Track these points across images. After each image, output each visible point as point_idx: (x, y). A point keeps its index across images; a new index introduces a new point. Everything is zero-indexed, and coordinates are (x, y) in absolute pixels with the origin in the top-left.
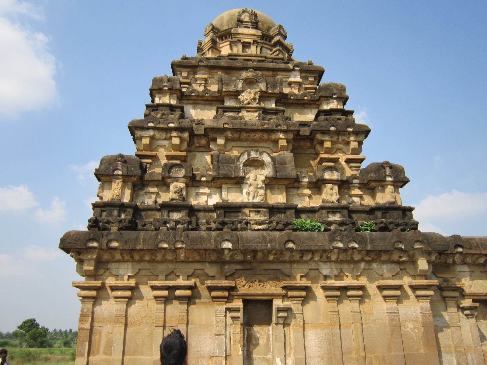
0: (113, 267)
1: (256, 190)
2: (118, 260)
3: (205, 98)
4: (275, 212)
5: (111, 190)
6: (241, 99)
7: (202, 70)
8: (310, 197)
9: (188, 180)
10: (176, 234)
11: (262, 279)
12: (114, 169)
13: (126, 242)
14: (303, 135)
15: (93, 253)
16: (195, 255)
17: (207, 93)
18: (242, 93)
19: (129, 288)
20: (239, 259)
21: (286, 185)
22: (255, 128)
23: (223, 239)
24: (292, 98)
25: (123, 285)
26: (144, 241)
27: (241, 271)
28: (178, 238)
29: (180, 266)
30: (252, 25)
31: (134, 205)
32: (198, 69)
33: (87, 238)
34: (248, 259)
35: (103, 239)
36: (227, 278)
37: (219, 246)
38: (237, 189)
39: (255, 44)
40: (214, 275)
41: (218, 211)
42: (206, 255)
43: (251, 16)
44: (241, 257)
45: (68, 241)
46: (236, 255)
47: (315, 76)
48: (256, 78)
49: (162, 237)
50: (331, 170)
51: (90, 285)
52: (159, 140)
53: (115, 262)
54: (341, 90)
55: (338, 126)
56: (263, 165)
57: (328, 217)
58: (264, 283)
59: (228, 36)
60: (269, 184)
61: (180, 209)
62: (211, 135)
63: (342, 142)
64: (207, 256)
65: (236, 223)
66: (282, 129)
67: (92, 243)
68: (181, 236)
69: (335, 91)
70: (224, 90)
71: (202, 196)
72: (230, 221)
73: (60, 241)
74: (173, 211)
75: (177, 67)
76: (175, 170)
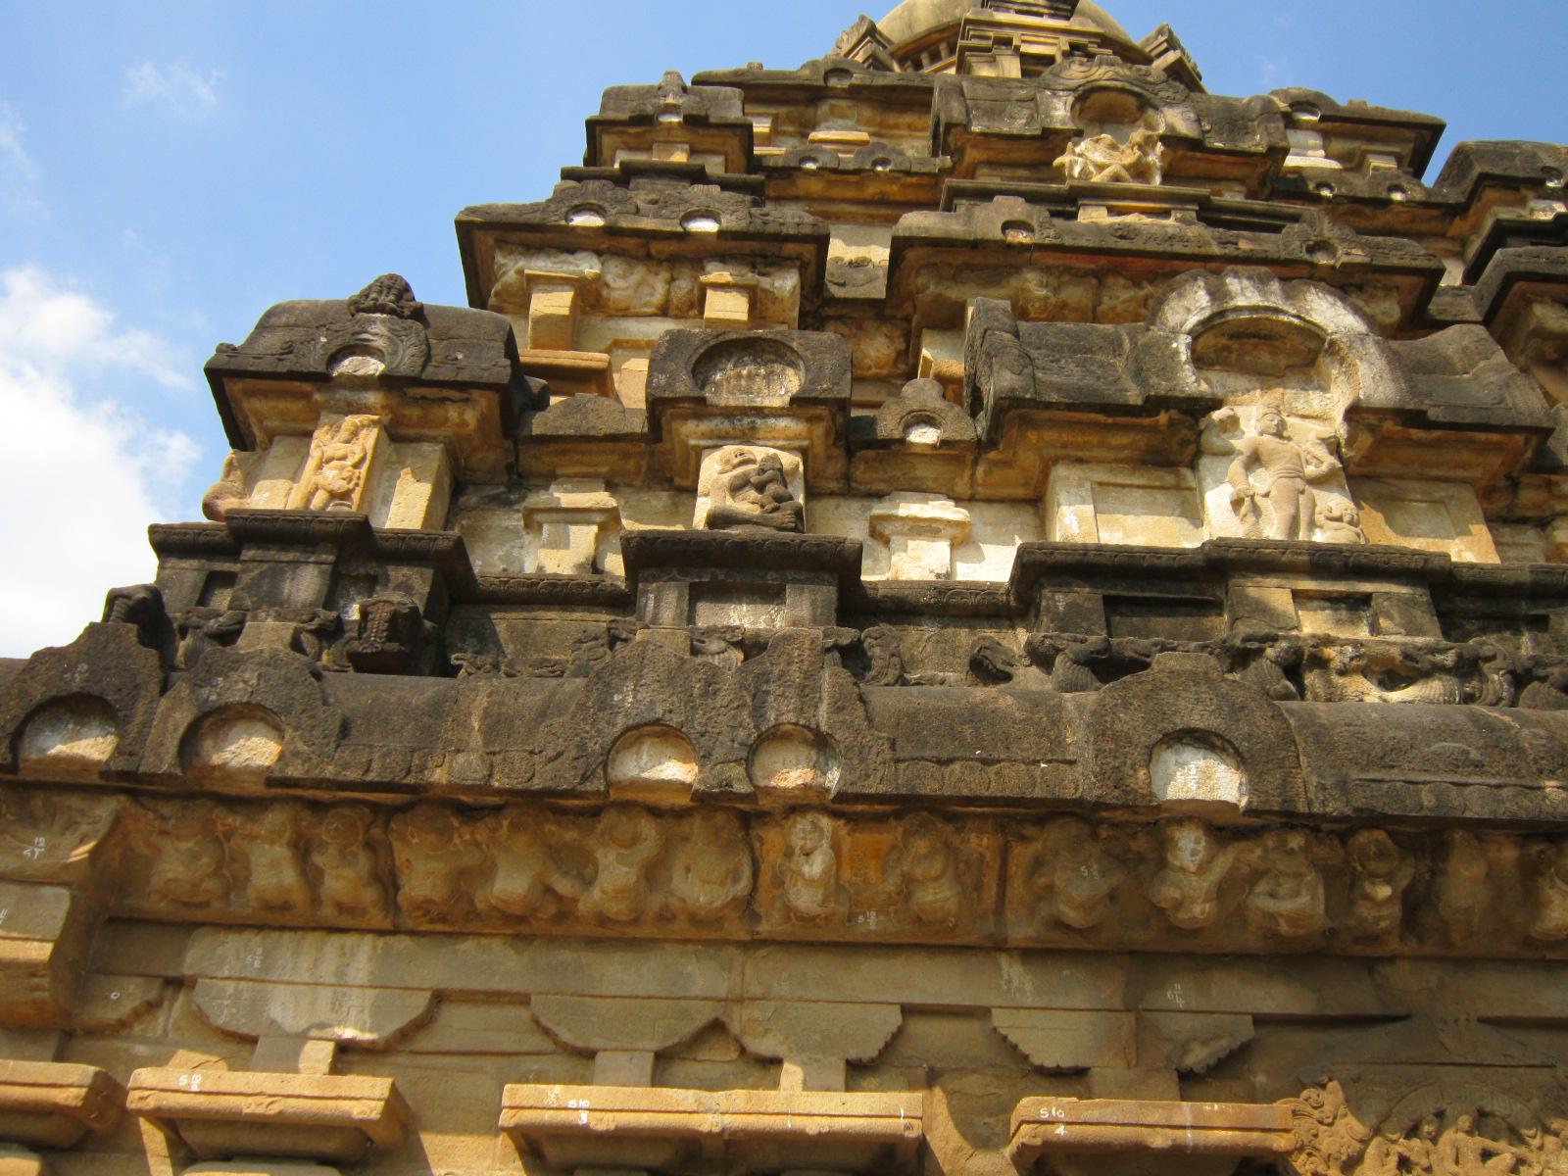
0: (224, 967)
2: (267, 906)
3: (871, 190)
6: (1071, 167)
7: (843, 116)
9: (819, 430)
10: (764, 677)
11: (1498, 1105)
12: (338, 343)
13: (345, 730)
15: (71, 825)
16: (918, 872)
17: (884, 162)
18: (1076, 144)
19: (330, 1146)
20: (1293, 920)
23: (1170, 728)
24: (1326, 193)
25: (275, 1109)
26: (496, 726)
27: (1303, 1038)
28: (782, 711)
29: (785, 979)
30: (1050, 8)
32: (824, 108)
33: (38, 693)
34: (1365, 911)
35: (164, 703)
36: (1190, 1082)
37: (1141, 774)
38: (1160, 496)
40: (1081, 1064)
41: (1059, 597)
42: (1003, 880)
44: (1314, 897)
46: (1262, 887)
48: (1136, 89)
52: (625, 313)
58: (1516, 1137)
59: (943, 47)
61: (772, 578)
64: (1017, 888)
66: (1345, 259)
67: (76, 736)
68: (807, 693)
69: (1549, 162)
70: (976, 128)
71: (912, 544)
74: (723, 593)
76: (739, 376)
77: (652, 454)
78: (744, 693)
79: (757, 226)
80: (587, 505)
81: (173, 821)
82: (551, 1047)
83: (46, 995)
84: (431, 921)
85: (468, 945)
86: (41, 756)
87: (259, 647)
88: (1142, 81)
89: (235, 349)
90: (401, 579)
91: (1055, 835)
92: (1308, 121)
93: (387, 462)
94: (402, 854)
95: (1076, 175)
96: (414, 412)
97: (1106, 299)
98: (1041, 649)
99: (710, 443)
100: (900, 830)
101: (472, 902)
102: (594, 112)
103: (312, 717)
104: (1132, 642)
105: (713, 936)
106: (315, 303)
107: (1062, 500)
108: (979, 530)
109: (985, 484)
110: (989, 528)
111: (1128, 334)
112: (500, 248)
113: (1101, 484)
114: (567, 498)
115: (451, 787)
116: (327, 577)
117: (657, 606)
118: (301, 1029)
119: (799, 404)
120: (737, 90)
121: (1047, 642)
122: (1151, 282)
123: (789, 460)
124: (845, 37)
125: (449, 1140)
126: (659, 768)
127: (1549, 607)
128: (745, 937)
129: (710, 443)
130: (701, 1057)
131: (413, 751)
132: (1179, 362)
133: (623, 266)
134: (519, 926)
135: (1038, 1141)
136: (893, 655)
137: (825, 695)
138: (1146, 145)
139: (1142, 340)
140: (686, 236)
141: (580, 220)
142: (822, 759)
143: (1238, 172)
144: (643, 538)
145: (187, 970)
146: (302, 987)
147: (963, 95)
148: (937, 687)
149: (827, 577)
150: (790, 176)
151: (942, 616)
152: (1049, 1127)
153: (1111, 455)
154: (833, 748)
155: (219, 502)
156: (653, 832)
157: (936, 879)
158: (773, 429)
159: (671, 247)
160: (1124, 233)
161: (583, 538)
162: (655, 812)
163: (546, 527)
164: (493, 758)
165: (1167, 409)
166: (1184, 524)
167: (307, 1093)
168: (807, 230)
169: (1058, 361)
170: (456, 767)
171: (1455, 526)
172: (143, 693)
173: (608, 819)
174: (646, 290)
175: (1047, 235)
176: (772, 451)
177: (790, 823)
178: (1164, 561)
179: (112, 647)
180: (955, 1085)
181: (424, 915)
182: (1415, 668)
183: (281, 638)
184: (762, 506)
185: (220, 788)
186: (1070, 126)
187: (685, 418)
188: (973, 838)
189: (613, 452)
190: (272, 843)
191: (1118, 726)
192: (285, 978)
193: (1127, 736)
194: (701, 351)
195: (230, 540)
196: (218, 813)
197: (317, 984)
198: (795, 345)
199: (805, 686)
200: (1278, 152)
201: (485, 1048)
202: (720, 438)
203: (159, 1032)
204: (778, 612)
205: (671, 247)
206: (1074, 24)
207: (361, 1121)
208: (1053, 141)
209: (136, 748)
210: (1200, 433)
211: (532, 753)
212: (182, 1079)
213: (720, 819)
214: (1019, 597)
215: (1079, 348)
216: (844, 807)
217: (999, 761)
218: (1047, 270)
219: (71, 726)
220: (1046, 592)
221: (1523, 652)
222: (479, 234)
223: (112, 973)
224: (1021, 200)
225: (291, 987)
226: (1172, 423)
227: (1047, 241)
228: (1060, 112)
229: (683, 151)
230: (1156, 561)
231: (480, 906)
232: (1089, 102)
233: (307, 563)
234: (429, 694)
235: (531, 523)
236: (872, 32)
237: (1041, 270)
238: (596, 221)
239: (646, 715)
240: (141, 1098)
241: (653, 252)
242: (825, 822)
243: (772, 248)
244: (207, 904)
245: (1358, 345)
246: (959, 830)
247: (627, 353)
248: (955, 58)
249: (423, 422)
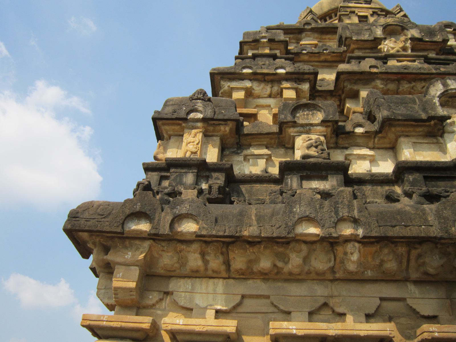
0: (181, 288)
2: (192, 271)
3: (322, 58)
5: (181, 149)
6: (384, 49)
7: (309, 37)
9: (329, 129)
10: (337, 203)
12: (189, 109)
15: (137, 249)
16: (385, 259)
17: (326, 50)
18: (385, 42)
26: (260, 218)
28: (344, 212)
30: (364, 1)
31: (227, 166)
32: (304, 35)
33: (128, 212)
38: (432, 146)
39: (375, 16)
40: (435, 314)
41: (410, 176)
42: (408, 261)
45: (86, 215)
48: (401, 24)
49: (303, 209)
51: (123, 325)
52: (259, 97)
53: (184, 277)
59: (333, 15)
61: (324, 173)
64: (413, 263)
68: (350, 207)
70: (354, 39)
71: (358, 162)
73: (69, 216)
74: (309, 178)
76: (304, 115)
77: (279, 138)
78: (332, 207)
79: (297, 70)
80: (262, 153)
81: (166, 247)
82: (277, 311)
83: (134, 297)
84: (239, 275)
85: (250, 282)
86: (129, 230)
87: (188, 197)
89: (159, 112)
90: (216, 176)
91: (425, 247)
92: (449, 31)
93: (204, 143)
94: (231, 255)
95: (385, 50)
96: (211, 128)
97: (401, 87)
98: (409, 192)
99: (297, 134)
100: (379, 246)
101: (252, 269)
102: (241, 39)
103: (207, 217)
104: (436, 189)
105: (322, 278)
106: (179, 98)
107: (403, 148)
108: (377, 157)
109: (378, 144)
110: (380, 156)
111: (417, 98)
112: (222, 80)
113: (414, 143)
114: (257, 152)
115: (250, 236)
116: (196, 176)
117: (291, 182)
118: (205, 306)
119: (324, 122)
120: (282, 31)
122: (414, 82)
123: (322, 138)
124: (302, 13)
125: (250, 338)
126: (308, 230)
128: (331, 278)
129: (297, 134)
130: (321, 313)
131: (237, 226)
132: (436, 106)
133: (258, 83)
134: (265, 276)
135: (430, 338)
136: (363, 195)
137: (356, 208)
138: (405, 41)
139: (424, 99)
140: (276, 74)
141: (245, 71)
142: (356, 226)
143: (433, 47)
144: (286, 163)
145: (170, 290)
146: (204, 294)
147: (349, 29)
148: (375, 204)
149: (340, 172)
151: (372, 183)
152: (433, 333)
153: (417, 134)
154: (359, 223)
155: (158, 156)
156: (306, 248)
157: (391, 260)
160: (406, 67)
161: (262, 163)
162: (305, 242)
163: (251, 160)
164: (261, 228)
165: (434, 120)
166: (441, 154)
167: (214, 325)
168: (312, 71)
169: (398, 107)
170: (251, 231)
172: (157, 211)
173: (292, 245)
174: (265, 90)
175: (383, 70)
176: (318, 136)
177: (346, 245)
178: (441, 165)
179: (146, 198)
180: (398, 321)
181: (238, 273)
183: (194, 195)
184: (318, 152)
185: (179, 238)
186: (383, 36)
187: (290, 127)
188: (400, 249)
189: (267, 138)
190: (195, 253)
191: (444, 215)
192: (199, 292)
193: (447, 218)
194: (293, 108)
195: (166, 167)
196: (179, 245)
197: (208, 293)
198: (320, 105)
199: (349, 205)
200: (446, 41)
201: (258, 311)
202: (300, 133)
203: (164, 307)
204: (326, 183)
206: (372, 5)
207: (230, 333)
208: (377, 41)
209: (158, 227)
210: (444, 127)
211: (272, 226)
212: (174, 321)
213: (325, 244)
214: (396, 177)
215: (403, 102)
216: (366, 241)
217: (410, 226)
218: (382, 79)
219: (136, 221)
220: (406, 175)
222: (216, 76)
223: (150, 291)
224: (374, 59)
225: (201, 294)
226: (435, 124)
227: (383, 71)
228: (379, 32)
229: (268, 49)
230: (438, 165)
231: (255, 270)
233: (189, 172)
234: (238, 210)
235: (246, 158)
236: (311, 11)
238: (249, 71)
239: (304, 214)
240: (166, 326)
241: (266, 79)
242: (357, 245)
243: (301, 76)
244: (175, 271)
246: (396, 246)
247: (260, 108)
249: (214, 131)
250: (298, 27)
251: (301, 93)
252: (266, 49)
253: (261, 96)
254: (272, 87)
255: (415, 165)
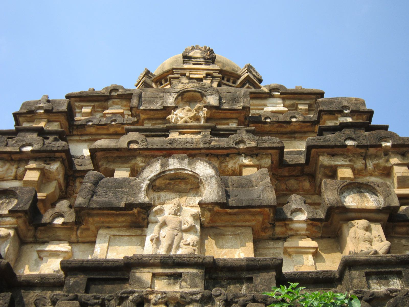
1: (176, 232)
3: (112, 130)
4: (222, 279)
6: (172, 119)
7: (117, 104)
8: (316, 255)
9: (20, 221)
14: (293, 163)
17: (115, 121)
18: (175, 111)
21: (255, 233)
22: (192, 147)
24: (268, 120)
30: (205, 62)
32: (110, 102)
38: (134, 239)
39: (208, 79)
43: (204, 53)
47: (308, 102)
48: (200, 90)
50: (359, 192)
54: (357, 104)
55: (361, 138)
56: (198, 187)
57: (369, 287)
60: (212, 227)
62: (104, 165)
63: (374, 171)
65: (112, 302)
66: (248, 146)
69: (346, 104)
70: (141, 108)
71: (49, 260)
72: (95, 298)
75: (76, 101)
88: (202, 87)
102: (17, 110)
109: (81, 237)
121: (54, 297)
127: (253, 274)
143: (235, 116)
150: (84, 127)
158: (5, 222)
159: (18, 156)
171: (241, 244)
174: (10, 171)
178: (110, 264)
182: (184, 301)
186: (173, 105)
205: (18, 156)
208: (167, 110)
221: (242, 292)
227: (142, 147)
228: (170, 100)
229: (44, 121)
230: (107, 264)
232: (184, 96)
237: (143, 157)
243: (52, 155)
245: (209, 180)
248: (169, 82)
250: (103, 94)
251: (50, 175)
252: (43, 121)
253: (5, 178)
254: (18, 167)
255: (80, 265)
